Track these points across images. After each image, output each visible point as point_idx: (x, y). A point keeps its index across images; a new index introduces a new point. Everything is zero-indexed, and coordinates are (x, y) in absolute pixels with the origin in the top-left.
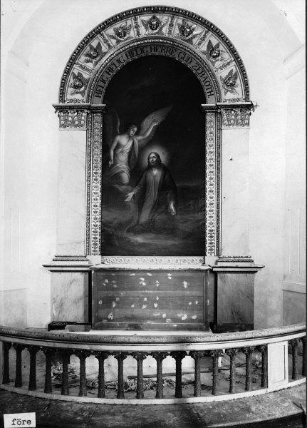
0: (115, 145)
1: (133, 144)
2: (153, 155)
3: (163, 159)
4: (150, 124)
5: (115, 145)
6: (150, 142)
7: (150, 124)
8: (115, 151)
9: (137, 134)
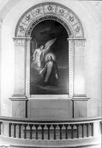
0: (35, 53)
1: (42, 53)
2: (49, 57)
3: (53, 58)
4: (48, 45)
5: (35, 53)
6: (48, 52)
7: (48, 45)
8: (35, 55)
9: (43, 48)
